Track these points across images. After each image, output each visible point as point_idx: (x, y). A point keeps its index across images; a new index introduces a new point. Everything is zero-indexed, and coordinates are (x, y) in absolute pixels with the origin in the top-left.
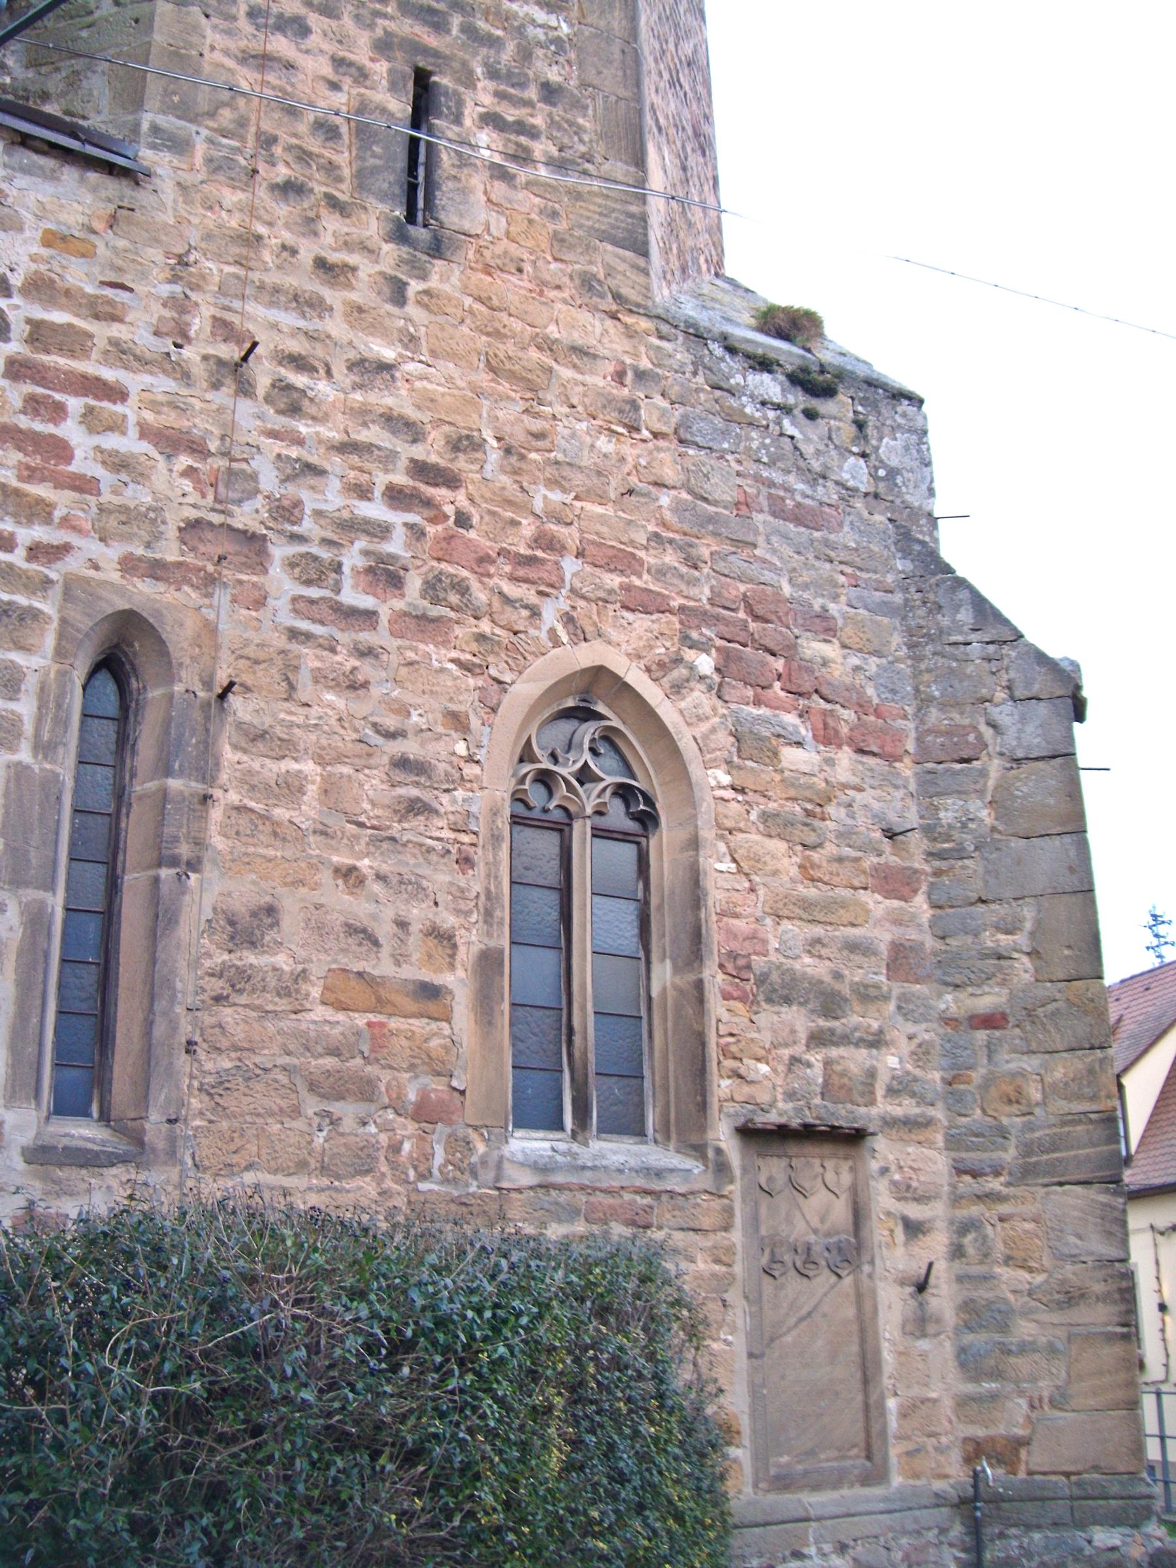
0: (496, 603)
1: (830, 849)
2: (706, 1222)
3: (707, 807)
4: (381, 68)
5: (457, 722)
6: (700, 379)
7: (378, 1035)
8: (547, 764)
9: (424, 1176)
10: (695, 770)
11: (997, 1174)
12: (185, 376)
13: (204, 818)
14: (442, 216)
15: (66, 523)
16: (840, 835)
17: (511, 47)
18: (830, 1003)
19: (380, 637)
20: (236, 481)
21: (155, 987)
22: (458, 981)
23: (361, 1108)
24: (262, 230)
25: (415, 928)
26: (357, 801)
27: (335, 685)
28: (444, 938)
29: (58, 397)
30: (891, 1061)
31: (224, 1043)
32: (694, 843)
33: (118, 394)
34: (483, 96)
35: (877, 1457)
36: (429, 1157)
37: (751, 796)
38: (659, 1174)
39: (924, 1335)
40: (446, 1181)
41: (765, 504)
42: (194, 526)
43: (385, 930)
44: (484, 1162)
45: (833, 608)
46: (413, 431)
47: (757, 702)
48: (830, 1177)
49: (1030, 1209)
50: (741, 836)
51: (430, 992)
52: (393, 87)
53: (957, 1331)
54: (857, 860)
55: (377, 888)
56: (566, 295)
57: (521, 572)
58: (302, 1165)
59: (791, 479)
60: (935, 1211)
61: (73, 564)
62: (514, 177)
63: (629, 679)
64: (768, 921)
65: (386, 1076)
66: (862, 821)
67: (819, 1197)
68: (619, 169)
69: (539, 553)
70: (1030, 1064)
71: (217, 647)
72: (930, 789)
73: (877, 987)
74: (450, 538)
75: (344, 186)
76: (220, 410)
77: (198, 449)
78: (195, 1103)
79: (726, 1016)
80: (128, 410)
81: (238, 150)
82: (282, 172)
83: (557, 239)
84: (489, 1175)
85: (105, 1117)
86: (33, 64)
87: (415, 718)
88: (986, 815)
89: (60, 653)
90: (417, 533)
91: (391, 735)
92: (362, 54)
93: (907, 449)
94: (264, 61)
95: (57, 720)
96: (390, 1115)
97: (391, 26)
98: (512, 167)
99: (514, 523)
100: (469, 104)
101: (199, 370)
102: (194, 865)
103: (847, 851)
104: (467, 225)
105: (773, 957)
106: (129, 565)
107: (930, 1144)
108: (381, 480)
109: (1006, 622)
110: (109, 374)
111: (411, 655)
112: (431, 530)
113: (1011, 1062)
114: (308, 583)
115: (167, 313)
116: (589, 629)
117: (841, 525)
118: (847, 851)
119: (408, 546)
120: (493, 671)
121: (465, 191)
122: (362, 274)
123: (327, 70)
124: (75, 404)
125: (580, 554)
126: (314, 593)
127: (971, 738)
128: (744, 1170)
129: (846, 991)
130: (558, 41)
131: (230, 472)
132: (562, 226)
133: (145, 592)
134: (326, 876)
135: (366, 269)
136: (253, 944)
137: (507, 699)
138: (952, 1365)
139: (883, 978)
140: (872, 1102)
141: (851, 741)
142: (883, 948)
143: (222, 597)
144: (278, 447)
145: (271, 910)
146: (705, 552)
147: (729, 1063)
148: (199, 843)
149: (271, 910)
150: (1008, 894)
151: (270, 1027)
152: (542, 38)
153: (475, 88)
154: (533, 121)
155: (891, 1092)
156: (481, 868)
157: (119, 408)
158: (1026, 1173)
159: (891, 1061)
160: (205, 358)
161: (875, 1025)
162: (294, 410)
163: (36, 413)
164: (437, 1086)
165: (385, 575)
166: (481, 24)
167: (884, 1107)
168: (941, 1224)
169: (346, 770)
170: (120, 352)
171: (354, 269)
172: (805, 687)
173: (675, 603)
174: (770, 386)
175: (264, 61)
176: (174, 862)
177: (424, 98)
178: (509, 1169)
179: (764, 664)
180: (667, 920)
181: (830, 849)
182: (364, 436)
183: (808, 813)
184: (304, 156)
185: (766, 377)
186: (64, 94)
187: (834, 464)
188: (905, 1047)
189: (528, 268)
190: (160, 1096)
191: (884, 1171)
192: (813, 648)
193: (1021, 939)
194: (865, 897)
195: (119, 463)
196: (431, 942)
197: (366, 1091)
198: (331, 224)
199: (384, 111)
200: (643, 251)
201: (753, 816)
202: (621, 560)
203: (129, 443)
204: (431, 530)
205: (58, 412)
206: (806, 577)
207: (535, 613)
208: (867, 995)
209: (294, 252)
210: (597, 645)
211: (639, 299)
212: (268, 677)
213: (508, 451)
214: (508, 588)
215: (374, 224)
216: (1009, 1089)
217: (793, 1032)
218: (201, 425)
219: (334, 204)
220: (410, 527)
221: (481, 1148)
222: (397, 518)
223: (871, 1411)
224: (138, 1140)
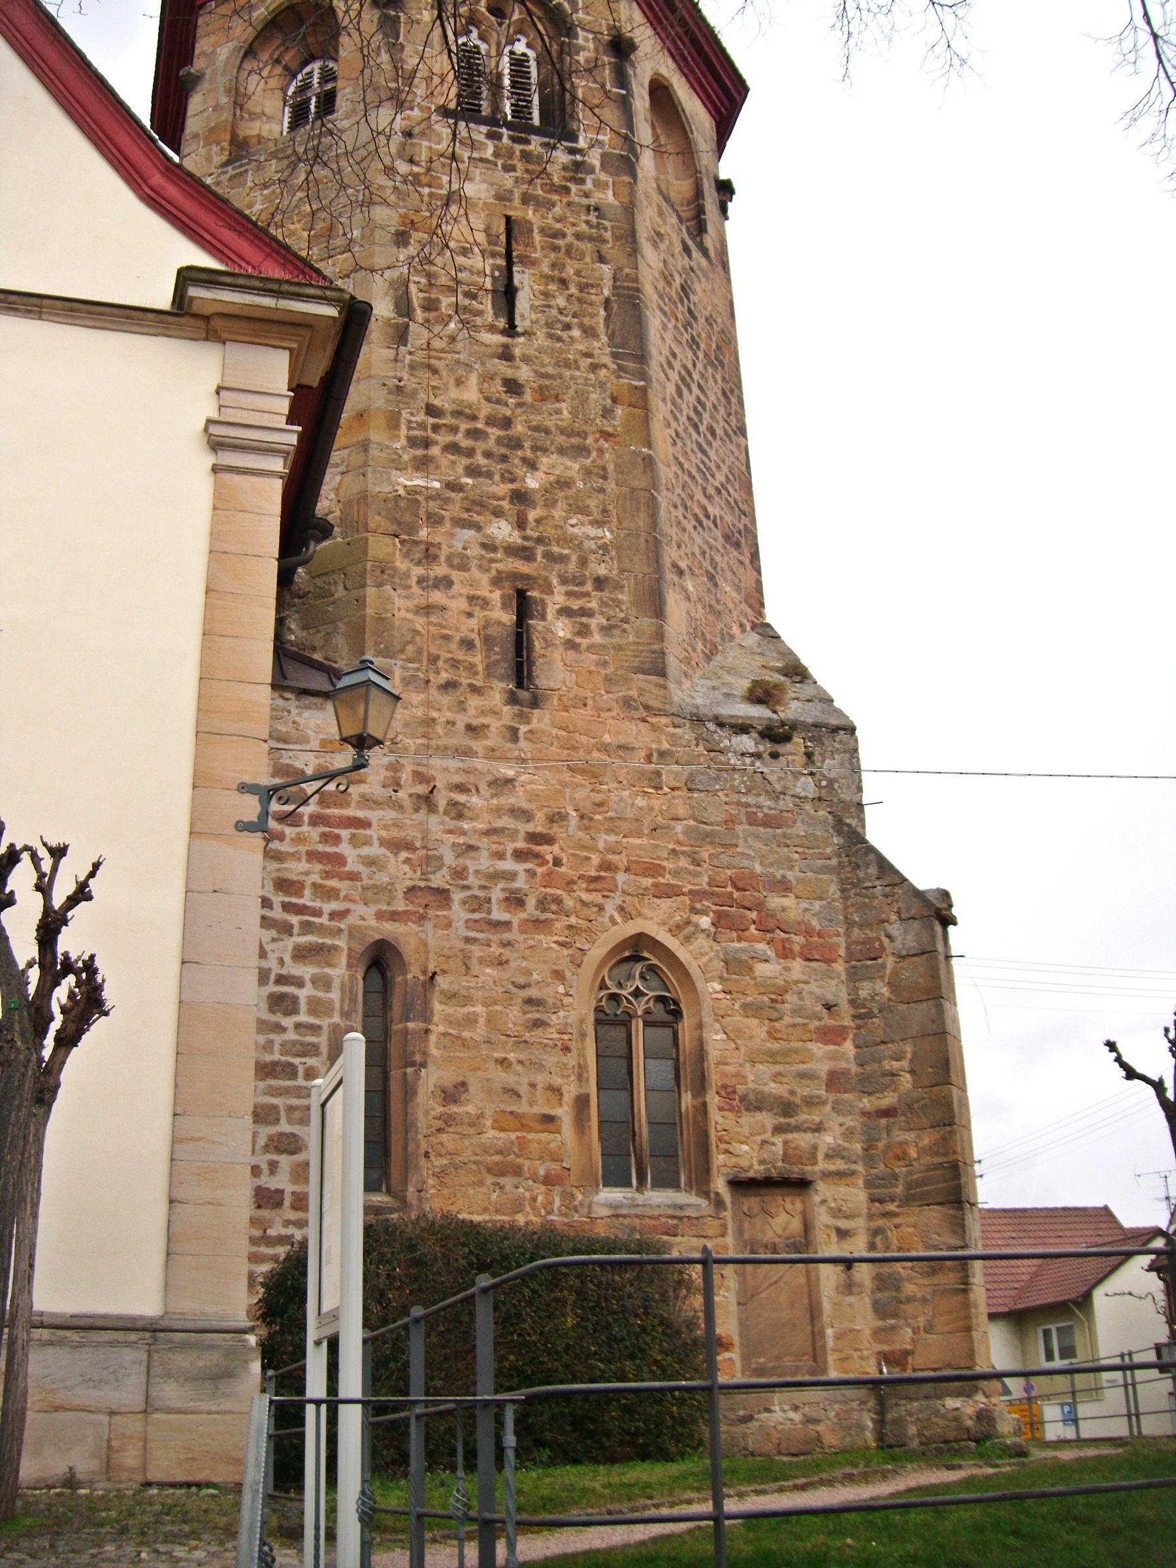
0: (579, 906)
1: (787, 1020)
2: (710, 1232)
3: (707, 1005)
4: (496, 596)
5: (559, 975)
6: (701, 748)
7: (522, 1143)
8: (614, 990)
9: (548, 1213)
10: (700, 984)
11: (893, 1201)
12: (400, 808)
13: (427, 1041)
14: (537, 682)
15: (347, 898)
16: (793, 1011)
17: (574, 558)
18: (787, 1108)
19: (514, 935)
20: (431, 862)
21: (408, 1126)
22: (564, 1112)
23: (515, 1180)
24: (435, 714)
25: (540, 1087)
26: (506, 1023)
27: (491, 964)
28: (556, 1091)
29: (336, 831)
30: (828, 1139)
31: (444, 1152)
32: (700, 1026)
33: (365, 824)
34: (558, 599)
35: (820, 1360)
36: (551, 1203)
37: (735, 995)
38: (681, 1208)
39: (851, 1294)
40: (561, 1214)
41: (744, 818)
42: (411, 890)
43: (523, 1089)
44: (581, 1204)
45: (790, 875)
46: (527, 816)
47: (740, 939)
48: (788, 1206)
49: (913, 1220)
50: (728, 1019)
51: (549, 1119)
52: (505, 606)
53: (873, 1292)
54: (805, 1025)
55: (518, 1068)
56: (614, 714)
57: (592, 886)
58: (485, 1210)
59: (761, 799)
60: (860, 1224)
61: (352, 919)
62: (579, 645)
63: (658, 938)
64: (748, 1065)
65: (527, 1163)
66: (808, 1002)
67: (783, 1218)
68: (646, 623)
69: (603, 874)
70: (910, 1136)
71: (427, 952)
72: (854, 976)
73: (819, 1097)
74: (550, 874)
75: (480, 677)
76: (420, 824)
77: (410, 847)
78: (430, 1182)
79: (720, 1120)
80: (372, 832)
81: (418, 669)
82: (444, 676)
83: (608, 679)
84: (585, 1211)
85: (389, 1192)
86: (305, 627)
87: (535, 976)
88: (885, 991)
89: (349, 966)
90: (531, 873)
91: (522, 987)
92: (484, 590)
93: (842, 764)
94: (427, 610)
95: (351, 1000)
96: (531, 1182)
97: (500, 566)
98: (578, 640)
99: (588, 859)
100: (550, 604)
101: (408, 804)
102: (423, 1065)
103: (799, 1020)
104: (552, 684)
105: (751, 1085)
106: (380, 916)
107: (855, 1186)
108: (510, 847)
109: (897, 872)
110: (361, 814)
111: (531, 942)
112: (539, 870)
113: (900, 1136)
114: (474, 911)
115: (389, 774)
116: (633, 913)
117: (795, 822)
118: (799, 1020)
119: (527, 882)
120: (578, 945)
121: (550, 663)
122: (493, 729)
123: (463, 605)
124: (345, 833)
125: (627, 870)
126: (477, 916)
127: (877, 945)
128: (733, 1204)
129: (798, 1101)
130: (604, 547)
131: (428, 857)
132: (610, 670)
133: (389, 929)
134: (491, 1064)
135: (495, 724)
136: (455, 1102)
137: (586, 959)
138: (870, 1310)
139: (823, 1092)
140: (815, 1163)
141: (802, 955)
142: (824, 1075)
143: (429, 925)
144: (451, 838)
145: (463, 1084)
146: (705, 855)
147: (723, 1146)
148: (425, 1053)
149: (463, 1084)
150: (897, 1037)
151: (466, 1142)
152: (594, 547)
153: (552, 593)
154: (589, 605)
155: (828, 1156)
156: (575, 1052)
157: (368, 832)
158: (908, 1200)
159: (828, 1139)
160: (410, 795)
161: (817, 1119)
162: (460, 816)
163: (326, 841)
164: (555, 1166)
165: (515, 901)
166: (556, 549)
167: (822, 1165)
168: (862, 1231)
169: (499, 1008)
170: (367, 801)
171: (488, 726)
172: (769, 925)
173: (685, 890)
174: (747, 743)
175: (427, 610)
176: (413, 1064)
177: (523, 606)
178: (595, 1207)
179: (743, 917)
180: (689, 1070)
181: (787, 1020)
182: (499, 823)
183: (773, 1001)
184: (454, 663)
185: (745, 737)
186: (322, 647)
187: (790, 784)
188: (838, 1131)
189: (590, 702)
190: (413, 1179)
191: (824, 1202)
192: (775, 902)
193: (905, 1064)
194: (809, 1045)
195: (371, 862)
196: (549, 1093)
197: (517, 1171)
198: (474, 702)
199: (499, 623)
200: (663, 674)
201: (737, 1006)
202: (653, 870)
203: (375, 850)
204: (539, 870)
205: (337, 839)
206: (771, 859)
207: (601, 908)
208: (812, 1102)
209: (454, 724)
210: (639, 920)
211: (660, 706)
212: (455, 965)
213: (582, 817)
214: (585, 896)
215: (498, 696)
216: (899, 1152)
217: (763, 1126)
218: (412, 834)
219: (474, 689)
220: (527, 871)
221: (580, 1197)
222: (520, 867)
223: (817, 1336)
224: (404, 1201)
